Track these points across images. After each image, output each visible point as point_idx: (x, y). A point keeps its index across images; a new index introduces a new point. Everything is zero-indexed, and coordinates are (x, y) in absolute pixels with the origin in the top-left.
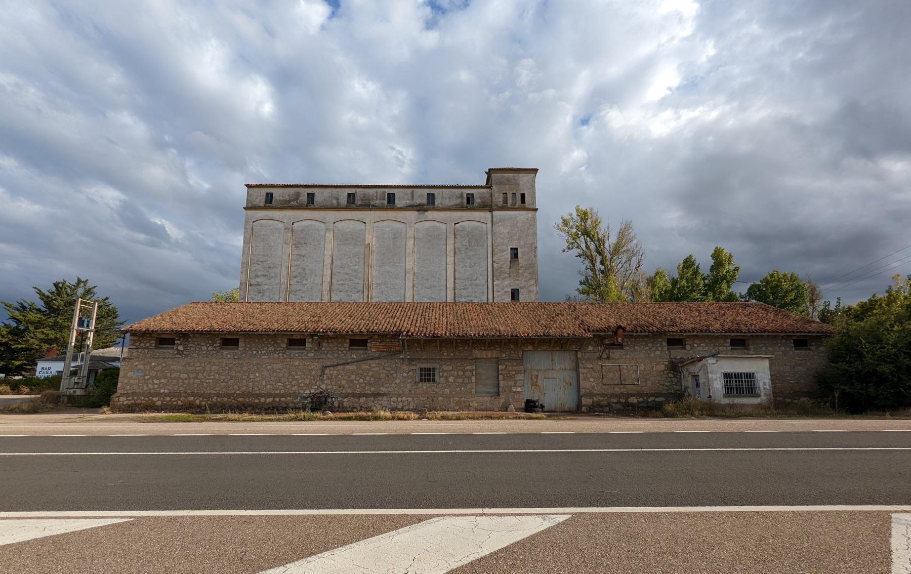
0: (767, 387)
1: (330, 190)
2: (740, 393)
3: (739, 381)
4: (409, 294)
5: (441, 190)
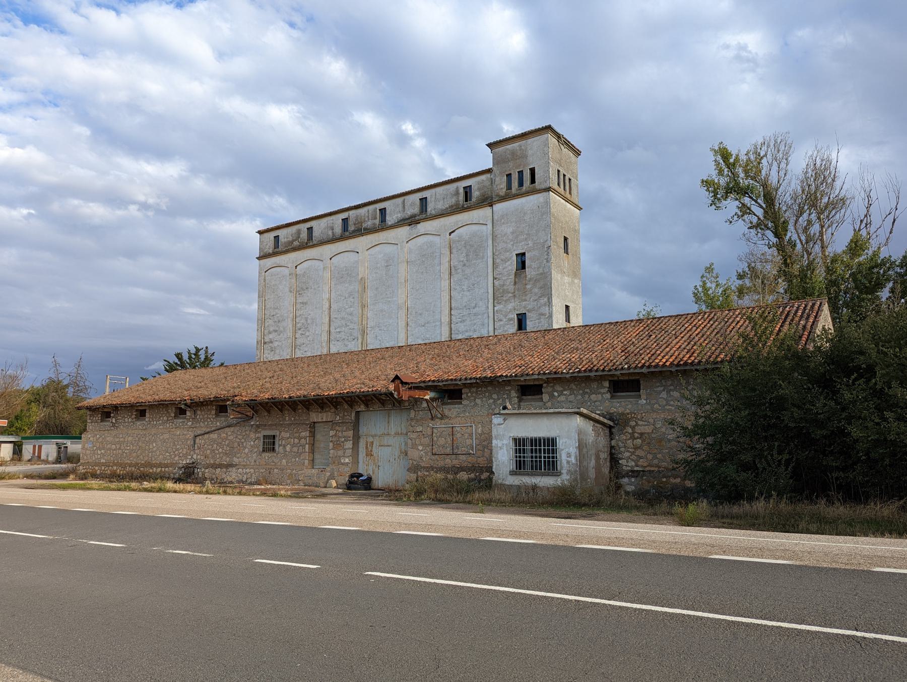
0: (573, 460)
1: (325, 220)
2: (536, 469)
4: (402, 336)
5: (433, 191)
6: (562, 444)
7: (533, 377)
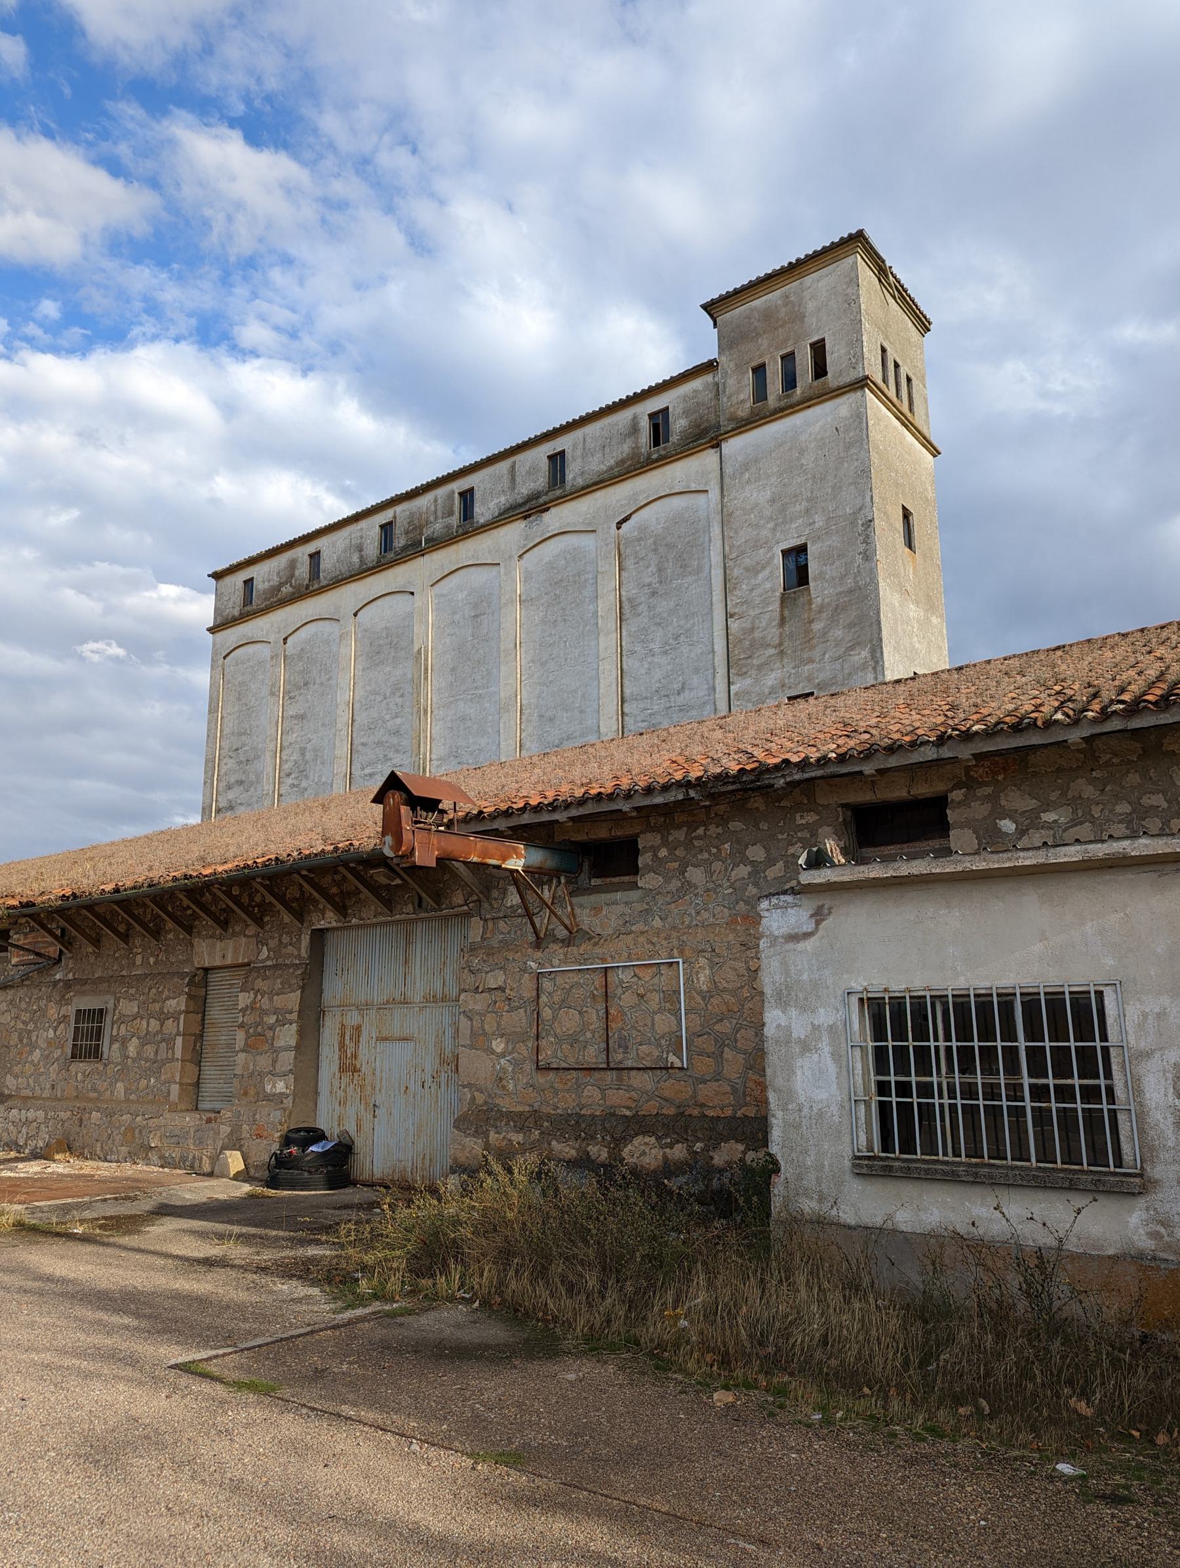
3: (988, 1054)
5: (578, 434)
6: (1141, 1026)
7: (916, 757)
